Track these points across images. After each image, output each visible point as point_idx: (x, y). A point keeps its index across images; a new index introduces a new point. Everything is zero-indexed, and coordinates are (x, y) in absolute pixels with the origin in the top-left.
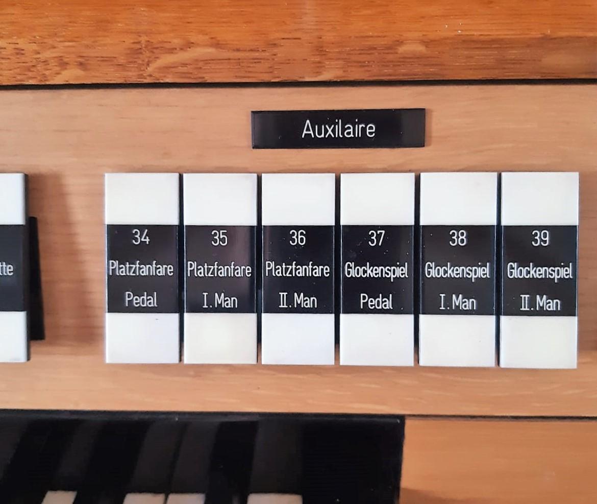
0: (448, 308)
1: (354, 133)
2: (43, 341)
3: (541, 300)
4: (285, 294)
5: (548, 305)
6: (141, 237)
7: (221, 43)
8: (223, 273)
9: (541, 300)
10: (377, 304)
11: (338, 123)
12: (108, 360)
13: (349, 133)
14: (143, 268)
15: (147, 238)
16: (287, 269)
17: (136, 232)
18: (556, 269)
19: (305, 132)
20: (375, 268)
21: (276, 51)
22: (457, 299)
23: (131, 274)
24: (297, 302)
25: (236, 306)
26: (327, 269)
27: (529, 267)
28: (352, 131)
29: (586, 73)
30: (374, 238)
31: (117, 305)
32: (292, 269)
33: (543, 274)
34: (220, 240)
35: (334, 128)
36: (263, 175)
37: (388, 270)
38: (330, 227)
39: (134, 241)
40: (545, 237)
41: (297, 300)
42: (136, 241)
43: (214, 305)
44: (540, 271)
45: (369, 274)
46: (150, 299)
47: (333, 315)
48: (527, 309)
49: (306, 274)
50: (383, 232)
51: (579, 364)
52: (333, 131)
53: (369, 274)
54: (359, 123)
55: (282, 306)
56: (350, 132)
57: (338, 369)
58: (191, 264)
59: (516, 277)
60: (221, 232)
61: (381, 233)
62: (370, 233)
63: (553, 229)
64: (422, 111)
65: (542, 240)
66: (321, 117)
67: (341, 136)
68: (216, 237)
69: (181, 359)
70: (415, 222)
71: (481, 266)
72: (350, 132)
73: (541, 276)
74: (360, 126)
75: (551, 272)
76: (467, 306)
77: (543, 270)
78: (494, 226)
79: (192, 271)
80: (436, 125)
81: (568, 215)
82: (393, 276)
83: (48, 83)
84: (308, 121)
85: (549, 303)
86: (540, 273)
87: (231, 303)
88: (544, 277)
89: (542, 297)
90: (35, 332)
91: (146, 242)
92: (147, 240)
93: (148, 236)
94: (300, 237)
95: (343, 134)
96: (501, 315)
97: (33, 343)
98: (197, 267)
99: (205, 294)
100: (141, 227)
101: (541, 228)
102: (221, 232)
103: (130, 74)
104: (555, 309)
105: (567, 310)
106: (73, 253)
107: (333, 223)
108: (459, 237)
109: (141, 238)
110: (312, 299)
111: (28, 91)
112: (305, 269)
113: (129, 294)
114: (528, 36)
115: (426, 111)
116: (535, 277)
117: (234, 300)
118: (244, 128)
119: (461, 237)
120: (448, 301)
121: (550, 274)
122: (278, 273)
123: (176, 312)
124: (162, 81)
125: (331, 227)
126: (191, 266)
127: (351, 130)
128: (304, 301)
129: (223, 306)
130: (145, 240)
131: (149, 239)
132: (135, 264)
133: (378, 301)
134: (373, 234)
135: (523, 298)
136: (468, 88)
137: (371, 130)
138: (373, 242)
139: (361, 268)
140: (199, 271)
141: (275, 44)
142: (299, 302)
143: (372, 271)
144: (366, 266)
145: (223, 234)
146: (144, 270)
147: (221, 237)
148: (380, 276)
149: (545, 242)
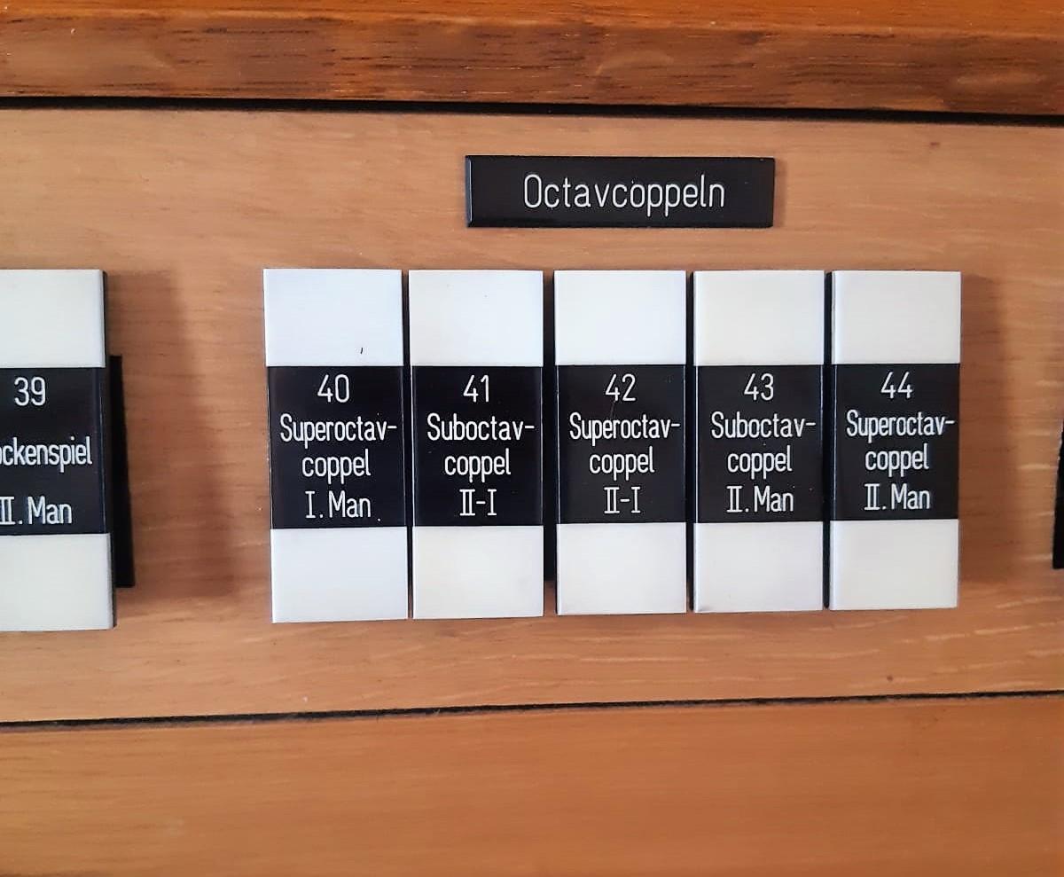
0: (321, 516)
2: (134, 589)
3: (899, 491)
4: (738, 488)
5: (911, 500)
9: (899, 491)
10: (67, 512)
12: (277, 616)
13: (582, 200)
17: (767, 378)
24: (759, 502)
28: (693, 195)
29: (98, 87)
31: (289, 514)
33: (39, 458)
36: (557, 274)
37: (54, 450)
38: (528, 371)
39: (17, 400)
41: (758, 499)
42: (20, 401)
44: (31, 451)
45: (19, 459)
47: (405, 528)
48: (875, 508)
53: (19, 459)
55: (869, 508)
56: (585, 197)
62: (17, 383)
64: (770, 162)
65: (32, 395)
66: (553, 167)
69: (691, 604)
70: (404, 363)
71: (75, 443)
72: (585, 197)
73: (35, 461)
75: (52, 454)
76: (779, 505)
77: (37, 450)
80: (793, 193)
82: (63, 462)
85: (776, 498)
86: (31, 455)
87: (918, 501)
89: (901, 488)
90: (123, 574)
91: (889, 394)
92: (909, 391)
95: (571, 201)
97: (118, 590)
99: (492, 491)
100: (898, 369)
101: (29, 373)
104: (921, 507)
105: (942, 508)
107: (400, 363)
108: (28, 390)
114: (635, 26)
115: (778, 168)
116: (23, 463)
118: (453, 190)
121: (50, 457)
125: (819, 366)
128: (771, 500)
130: (887, 391)
131: (619, 391)
134: (21, 384)
135: (3, 503)
136: (255, 118)
139: (906, 434)
141: (208, 31)
142: (762, 503)
143: (23, 453)
148: (39, 463)
149: (38, 398)
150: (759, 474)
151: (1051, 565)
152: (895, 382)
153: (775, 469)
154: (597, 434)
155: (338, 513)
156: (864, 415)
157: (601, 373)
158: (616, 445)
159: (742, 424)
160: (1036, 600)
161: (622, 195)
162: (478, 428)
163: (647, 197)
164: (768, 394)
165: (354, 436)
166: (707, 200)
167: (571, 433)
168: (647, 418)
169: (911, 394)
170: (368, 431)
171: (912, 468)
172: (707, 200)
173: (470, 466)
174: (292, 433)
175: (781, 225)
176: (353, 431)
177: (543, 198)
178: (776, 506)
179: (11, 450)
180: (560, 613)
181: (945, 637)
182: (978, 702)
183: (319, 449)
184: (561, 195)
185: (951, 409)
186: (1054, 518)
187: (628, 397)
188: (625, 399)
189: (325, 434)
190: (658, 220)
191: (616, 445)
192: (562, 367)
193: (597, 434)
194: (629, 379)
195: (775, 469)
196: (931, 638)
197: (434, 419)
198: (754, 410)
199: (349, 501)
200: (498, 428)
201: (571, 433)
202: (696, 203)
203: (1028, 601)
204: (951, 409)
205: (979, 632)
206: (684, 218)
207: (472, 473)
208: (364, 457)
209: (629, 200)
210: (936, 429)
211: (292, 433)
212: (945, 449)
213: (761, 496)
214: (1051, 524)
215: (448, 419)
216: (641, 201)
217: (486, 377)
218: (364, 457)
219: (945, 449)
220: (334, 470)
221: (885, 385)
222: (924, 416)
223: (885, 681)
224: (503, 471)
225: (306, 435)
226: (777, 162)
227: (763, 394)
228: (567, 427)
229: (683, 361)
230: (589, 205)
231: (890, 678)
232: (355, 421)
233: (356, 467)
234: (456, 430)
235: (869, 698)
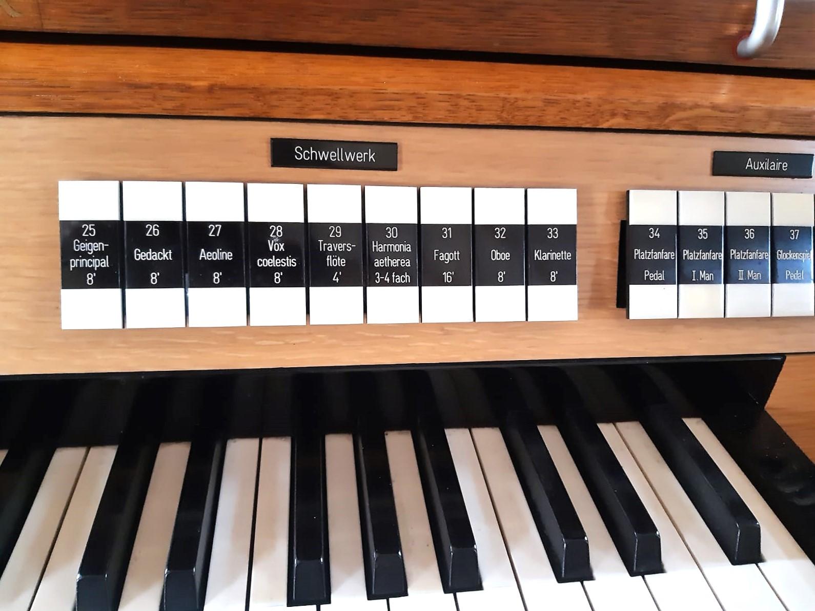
1: (775, 168)
6: (654, 233)
7: (520, 103)
8: (705, 257)
11: (767, 161)
14: (655, 254)
16: (648, 254)
17: (651, 230)
18: (803, 254)
19: (748, 166)
21: (74, 96)
23: (648, 258)
25: (409, 281)
26: (673, 254)
27: (162, 252)
28: (775, 166)
30: (793, 234)
32: (651, 255)
34: (703, 235)
35: (765, 164)
40: (338, 231)
43: (699, 279)
46: (660, 275)
49: (554, 258)
50: (220, 226)
51: (579, 318)
52: (764, 166)
54: (778, 162)
57: (187, 331)
58: (637, 251)
60: (90, 225)
61: (218, 227)
63: (561, 227)
64: (395, 145)
66: (307, 144)
67: (768, 169)
68: (701, 233)
74: (779, 163)
78: (768, 227)
79: (637, 256)
80: (404, 155)
81: (569, 217)
83: (598, 127)
84: (750, 159)
92: (658, 235)
94: (751, 233)
95: (769, 168)
98: (542, 253)
99: (694, 271)
100: (655, 227)
102: (90, 225)
103: (653, 123)
109: (276, 229)
110: (710, 274)
111: (680, 136)
113: (647, 272)
117: (711, 276)
119: (278, 231)
120: (698, 275)
122: (642, 257)
124: (670, 129)
125: (470, 225)
126: (686, 252)
127: (774, 166)
132: (651, 251)
133: (656, 275)
137: (785, 166)
138: (792, 236)
140: (674, 255)
144: (789, 252)
145: (705, 231)
146: (545, 256)
149: (338, 234)
155: (703, 279)
159: (499, 255)
177: (303, 156)
179: (162, 254)
188: (502, 237)
189: (342, 248)
191: (335, 254)
202: (362, 160)
207: (96, 266)
208: (272, 259)
217: (450, 229)
218: (272, 259)
226: (398, 144)
229: (471, 223)
233: (393, 263)
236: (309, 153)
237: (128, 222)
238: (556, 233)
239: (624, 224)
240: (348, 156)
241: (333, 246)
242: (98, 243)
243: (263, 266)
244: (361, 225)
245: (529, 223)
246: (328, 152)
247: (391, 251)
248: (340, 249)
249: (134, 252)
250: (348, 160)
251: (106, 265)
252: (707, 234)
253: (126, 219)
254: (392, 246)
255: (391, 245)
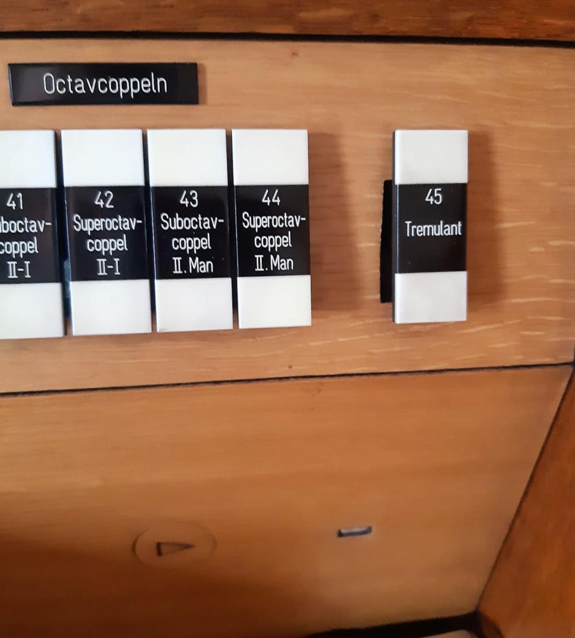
9: (275, 259)
13: (79, 89)
15: (14, 202)
20: (419, 226)
22: (275, 259)
25: (292, 268)
28: (146, 85)
43: (269, 268)
48: (180, 272)
57: (154, 335)
59: (442, 235)
64: (194, 66)
66: (63, 69)
81: (458, 174)
88: (424, 235)
92: (278, 201)
93: (187, 198)
95: (73, 89)
96: (396, 273)
100: (271, 188)
106: (343, 214)
110: (288, 260)
112: (454, 227)
115: (199, 67)
117: (290, 262)
123: (57, 281)
129: (279, 269)
130: (429, 200)
142: (194, 267)
145: (438, 192)
147: (436, 195)
150: (17, 255)
151: (380, 301)
152: (270, 196)
153: (117, 249)
154: (258, 224)
155: (194, 270)
156: (252, 215)
157: (92, 191)
158: (270, 231)
160: (371, 321)
161: (104, 85)
162: (191, 222)
163: (120, 86)
164: (194, 202)
165: (197, 226)
166: (156, 88)
167: (244, 224)
168: (201, 217)
169: (280, 203)
170: (32, 226)
171: (28, 252)
172: (156, 88)
173: (103, 246)
174: (81, 226)
175: (205, 103)
176: (282, 221)
178: (202, 269)
180: (398, 320)
181: (321, 343)
182: (342, 379)
183: (96, 235)
184: (66, 86)
185: (305, 213)
186: (379, 274)
187: (110, 204)
190: (127, 100)
191: (270, 231)
192: (237, 187)
193: (258, 224)
194: (109, 195)
195: (201, 247)
196: (312, 344)
197: (77, 219)
198: (186, 212)
199: (200, 263)
200: (29, 225)
201: (244, 224)
203: (367, 321)
204: (305, 213)
205: (340, 340)
206: (142, 99)
207: (104, 249)
209: (108, 88)
210: (130, 226)
211: (81, 226)
212: (301, 235)
213: (194, 264)
214: (379, 276)
215: (172, 216)
216: (52, 89)
219: (301, 235)
220: (190, 245)
221: (10, 201)
222: (202, 217)
223: (287, 368)
224: (287, 245)
225: (257, 224)
227: (191, 203)
228: (241, 220)
230: (85, 92)
231: (290, 367)
232: (197, 217)
233: (283, 241)
234: (178, 223)
235: (280, 379)
236: (106, 82)
237: (158, 189)
238: (195, 198)
239: (389, 185)
240: (92, 87)
241: (130, 222)
242: (422, 226)
243: (95, 250)
244: (227, 188)
245: (68, 182)
246: (95, 80)
247: (428, 234)
248: (420, 233)
249: (171, 242)
250: (92, 91)
251: (287, 267)
252: (441, 197)
253: (153, 183)
254: (431, 228)
255: (428, 227)
